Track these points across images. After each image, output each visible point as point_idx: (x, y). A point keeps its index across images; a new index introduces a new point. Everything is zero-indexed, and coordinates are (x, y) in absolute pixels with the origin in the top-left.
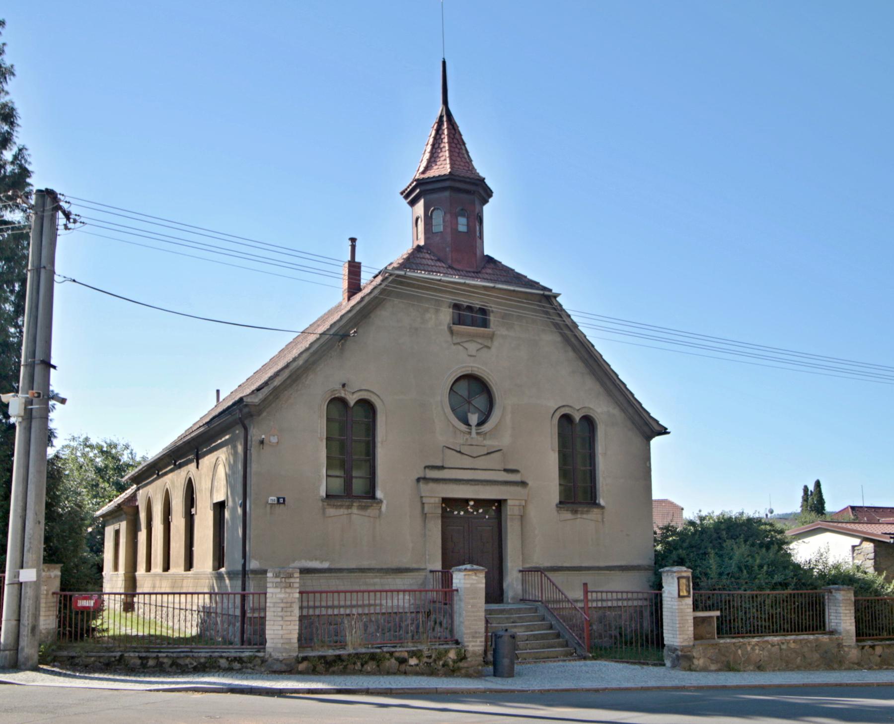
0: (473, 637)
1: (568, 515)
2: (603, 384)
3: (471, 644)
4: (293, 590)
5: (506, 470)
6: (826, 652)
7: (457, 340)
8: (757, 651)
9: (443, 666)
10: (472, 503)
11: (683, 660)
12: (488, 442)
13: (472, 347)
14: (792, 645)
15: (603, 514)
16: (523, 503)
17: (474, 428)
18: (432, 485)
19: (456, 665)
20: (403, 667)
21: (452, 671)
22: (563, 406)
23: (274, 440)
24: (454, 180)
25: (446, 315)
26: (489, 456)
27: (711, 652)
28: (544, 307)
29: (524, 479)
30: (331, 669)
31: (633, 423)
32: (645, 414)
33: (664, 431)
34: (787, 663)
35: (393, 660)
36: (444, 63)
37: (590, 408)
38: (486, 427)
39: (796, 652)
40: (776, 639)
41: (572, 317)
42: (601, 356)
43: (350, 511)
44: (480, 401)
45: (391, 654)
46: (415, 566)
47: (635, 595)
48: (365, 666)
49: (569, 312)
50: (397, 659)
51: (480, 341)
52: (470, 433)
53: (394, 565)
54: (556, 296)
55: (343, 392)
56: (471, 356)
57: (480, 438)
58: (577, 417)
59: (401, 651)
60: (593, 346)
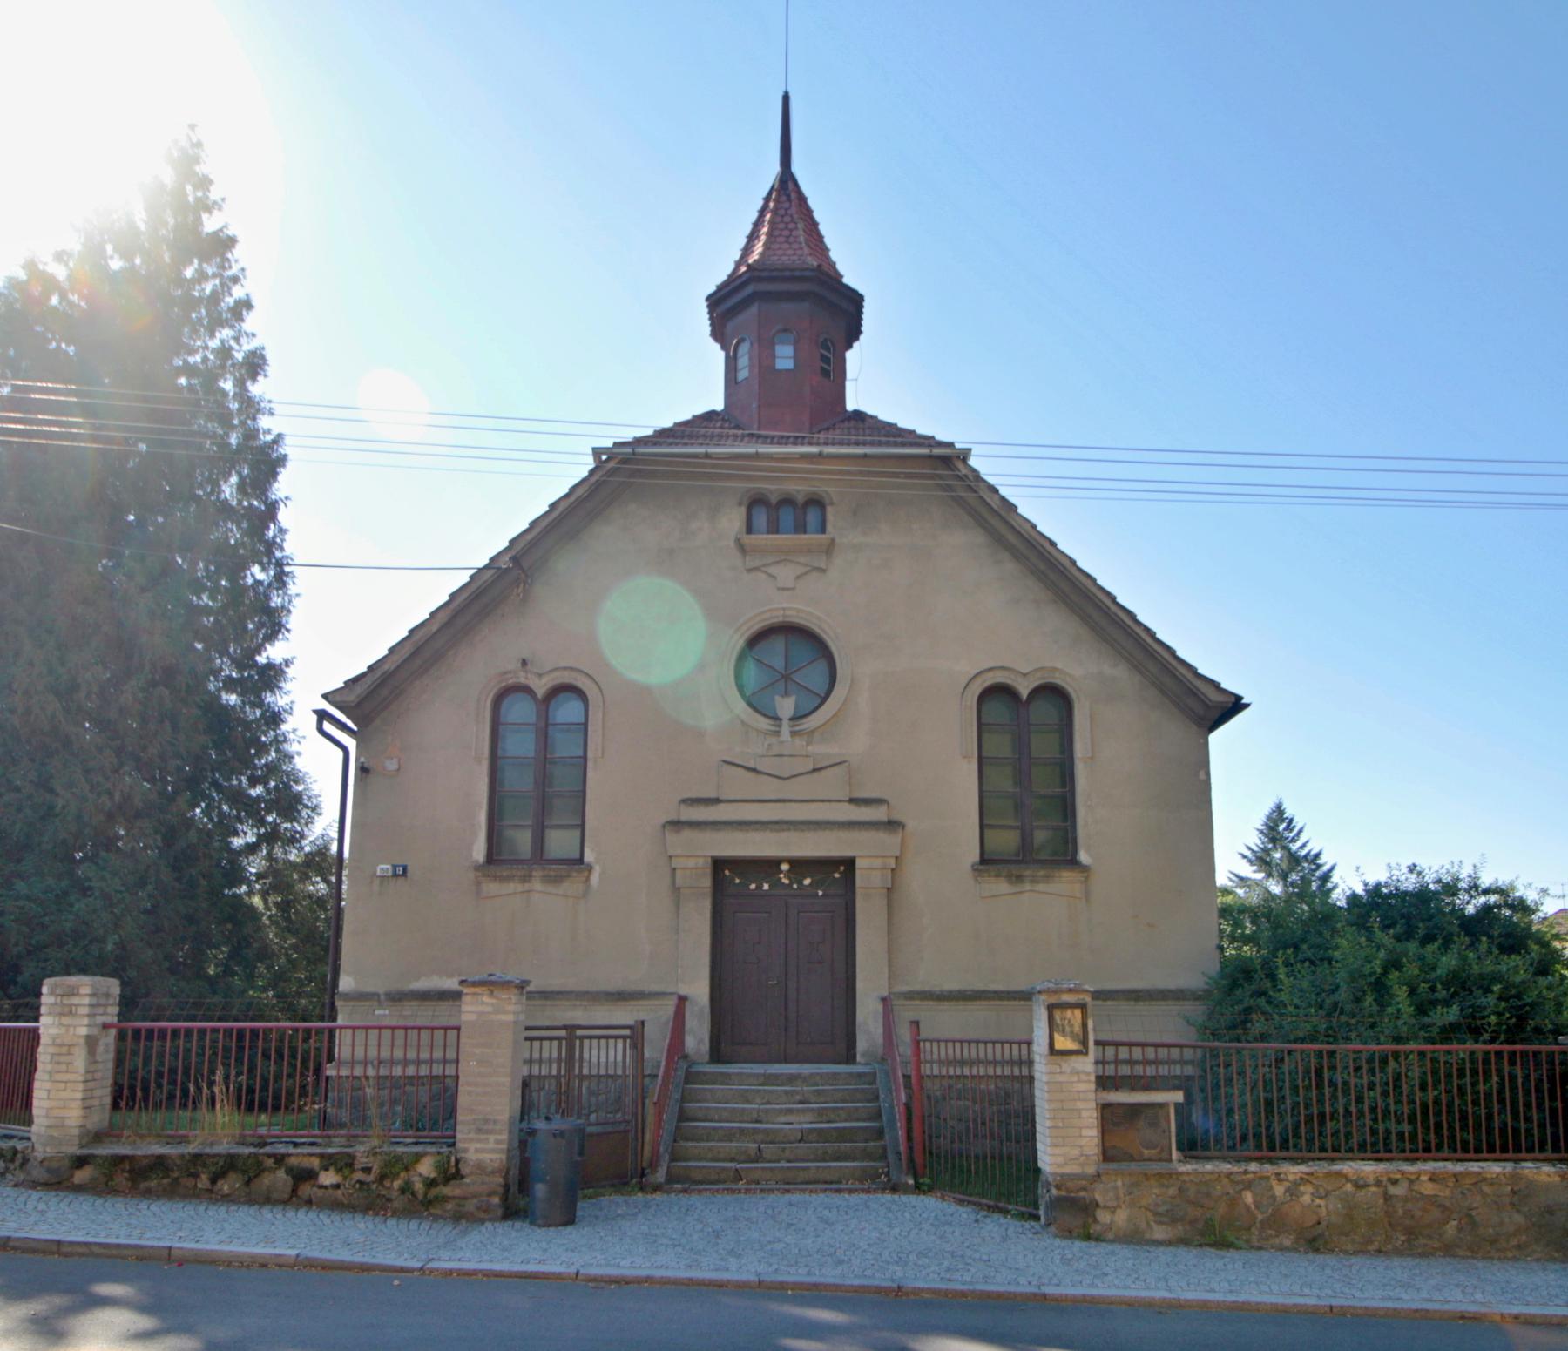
0: (479, 1131)
1: (1003, 887)
2: (1085, 619)
3: (473, 1146)
4: (77, 1021)
6: (1550, 1211)
7: (752, 562)
8: (1306, 1199)
9: (403, 1191)
10: (785, 867)
11: (1074, 1214)
13: (786, 574)
14: (1428, 1189)
15: (1087, 878)
16: (892, 863)
17: (786, 728)
18: (687, 833)
19: (434, 1192)
20: (306, 1190)
21: (422, 1204)
22: (991, 669)
23: (392, 765)
24: (760, 279)
25: (732, 520)
26: (816, 775)
27: (1153, 1194)
28: (940, 477)
29: (896, 816)
30: (143, 1185)
31: (1163, 693)
32: (1184, 671)
34: (1411, 1233)
35: (281, 1174)
36: (786, 98)
37: (1054, 669)
39: (1443, 1208)
40: (1370, 1169)
41: (1003, 492)
42: (1073, 562)
43: (527, 886)
44: (814, 676)
45: (280, 1159)
46: (655, 988)
47: (1175, 1053)
48: (219, 1183)
49: (992, 480)
50: (290, 1171)
51: (802, 559)
52: (777, 733)
53: (611, 986)
54: (964, 455)
55: (522, 674)
56: (783, 589)
57: (798, 742)
59: (303, 1157)
60: (1053, 544)
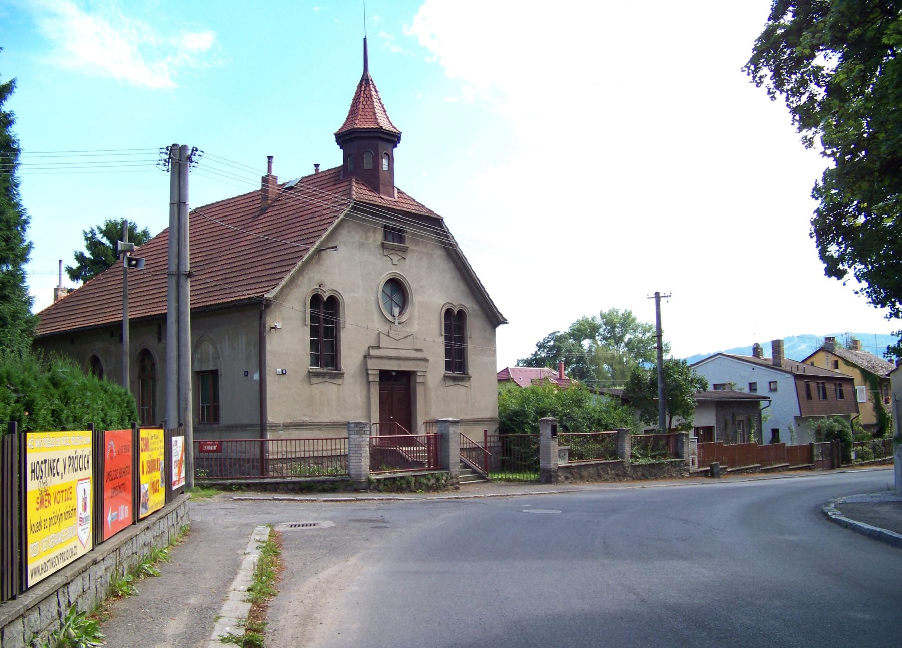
12: (404, 329)
33: (504, 322)
36: (365, 39)
38: (404, 318)
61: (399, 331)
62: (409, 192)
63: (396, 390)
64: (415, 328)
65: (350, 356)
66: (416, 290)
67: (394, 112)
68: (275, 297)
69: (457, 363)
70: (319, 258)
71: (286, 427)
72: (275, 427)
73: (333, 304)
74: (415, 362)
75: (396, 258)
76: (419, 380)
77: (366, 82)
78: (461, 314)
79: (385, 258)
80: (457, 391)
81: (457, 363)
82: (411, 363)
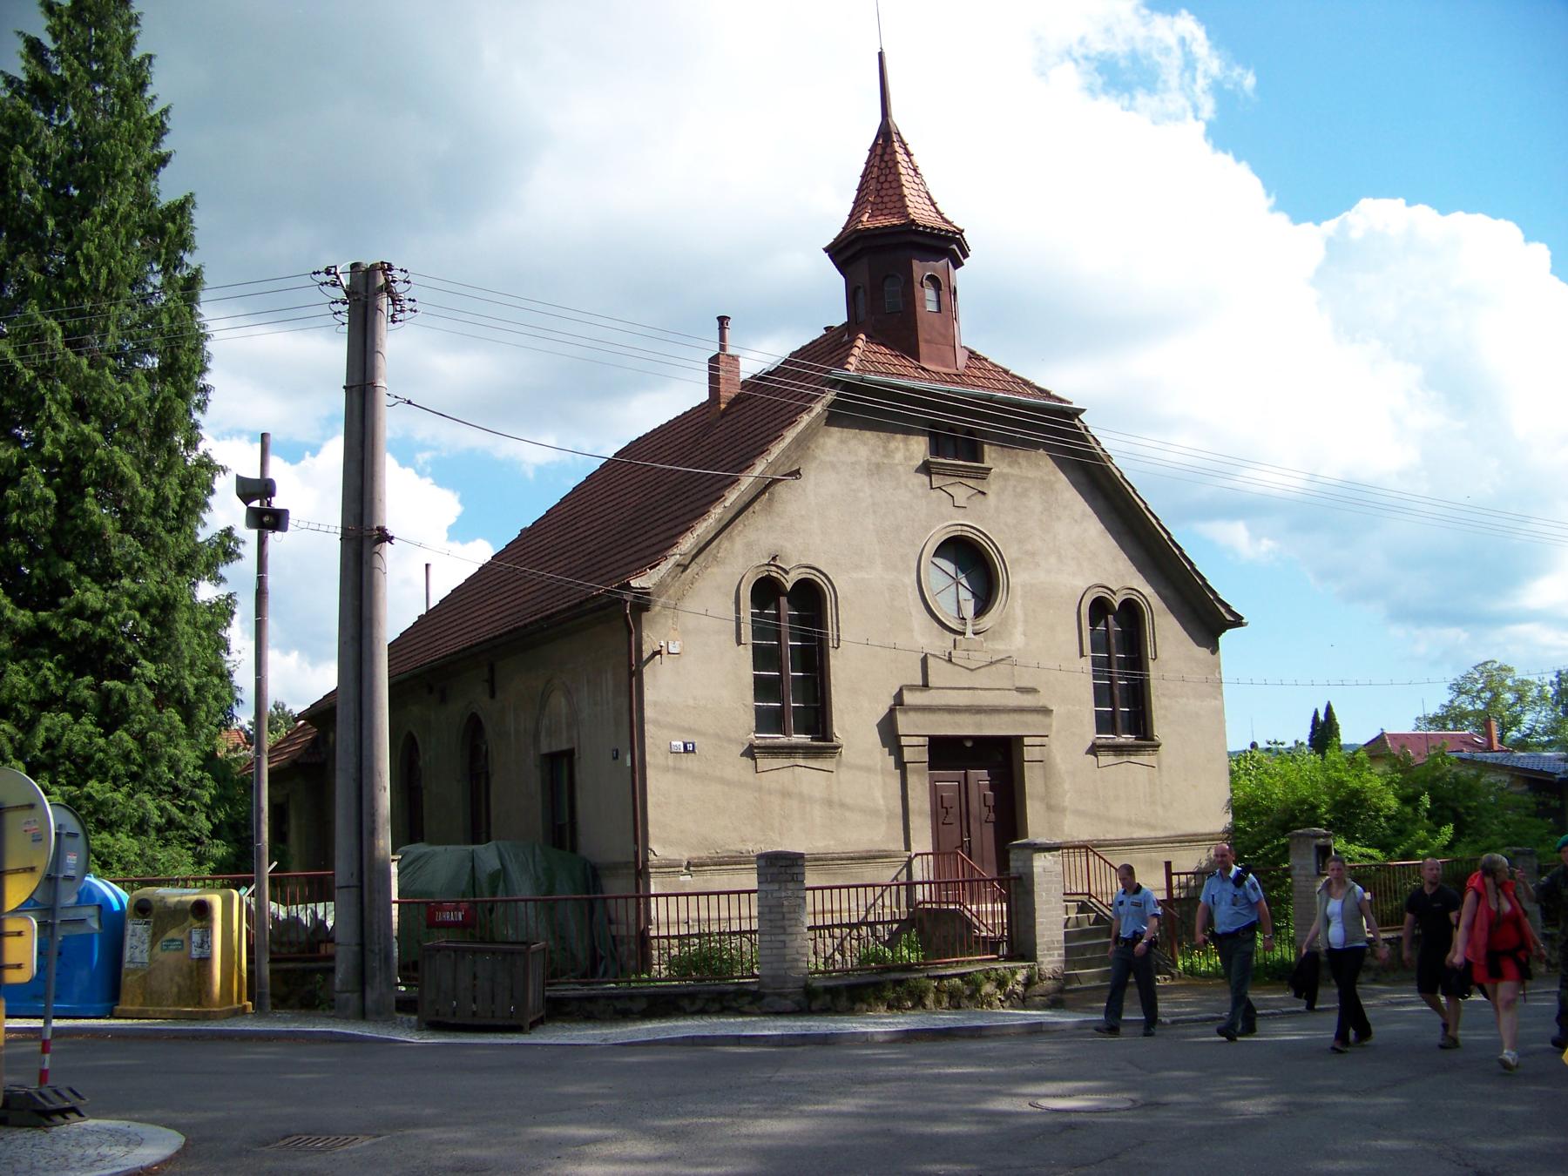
5: (1020, 690)
12: (988, 645)
33: (1238, 622)
36: (881, 55)
38: (988, 621)
58: (1116, 602)
61: (977, 650)
62: (997, 356)
63: (982, 773)
64: (1016, 642)
65: (855, 711)
66: (1016, 561)
67: (944, 187)
68: (661, 584)
69: (1127, 714)
70: (770, 500)
71: (693, 866)
72: (671, 867)
73: (810, 600)
74: (1016, 717)
75: (961, 493)
76: (1028, 754)
77: (886, 138)
78: (1131, 612)
79: (935, 494)
80: (1130, 773)
81: (1127, 714)
82: (1005, 718)
